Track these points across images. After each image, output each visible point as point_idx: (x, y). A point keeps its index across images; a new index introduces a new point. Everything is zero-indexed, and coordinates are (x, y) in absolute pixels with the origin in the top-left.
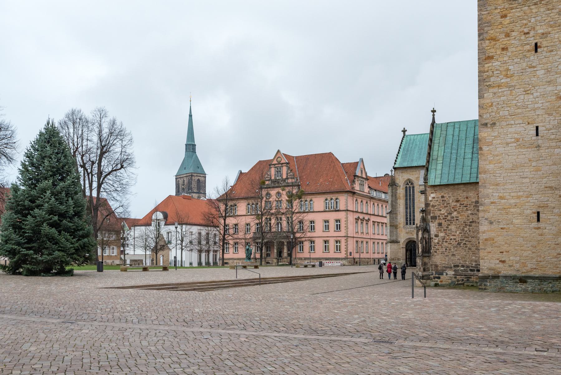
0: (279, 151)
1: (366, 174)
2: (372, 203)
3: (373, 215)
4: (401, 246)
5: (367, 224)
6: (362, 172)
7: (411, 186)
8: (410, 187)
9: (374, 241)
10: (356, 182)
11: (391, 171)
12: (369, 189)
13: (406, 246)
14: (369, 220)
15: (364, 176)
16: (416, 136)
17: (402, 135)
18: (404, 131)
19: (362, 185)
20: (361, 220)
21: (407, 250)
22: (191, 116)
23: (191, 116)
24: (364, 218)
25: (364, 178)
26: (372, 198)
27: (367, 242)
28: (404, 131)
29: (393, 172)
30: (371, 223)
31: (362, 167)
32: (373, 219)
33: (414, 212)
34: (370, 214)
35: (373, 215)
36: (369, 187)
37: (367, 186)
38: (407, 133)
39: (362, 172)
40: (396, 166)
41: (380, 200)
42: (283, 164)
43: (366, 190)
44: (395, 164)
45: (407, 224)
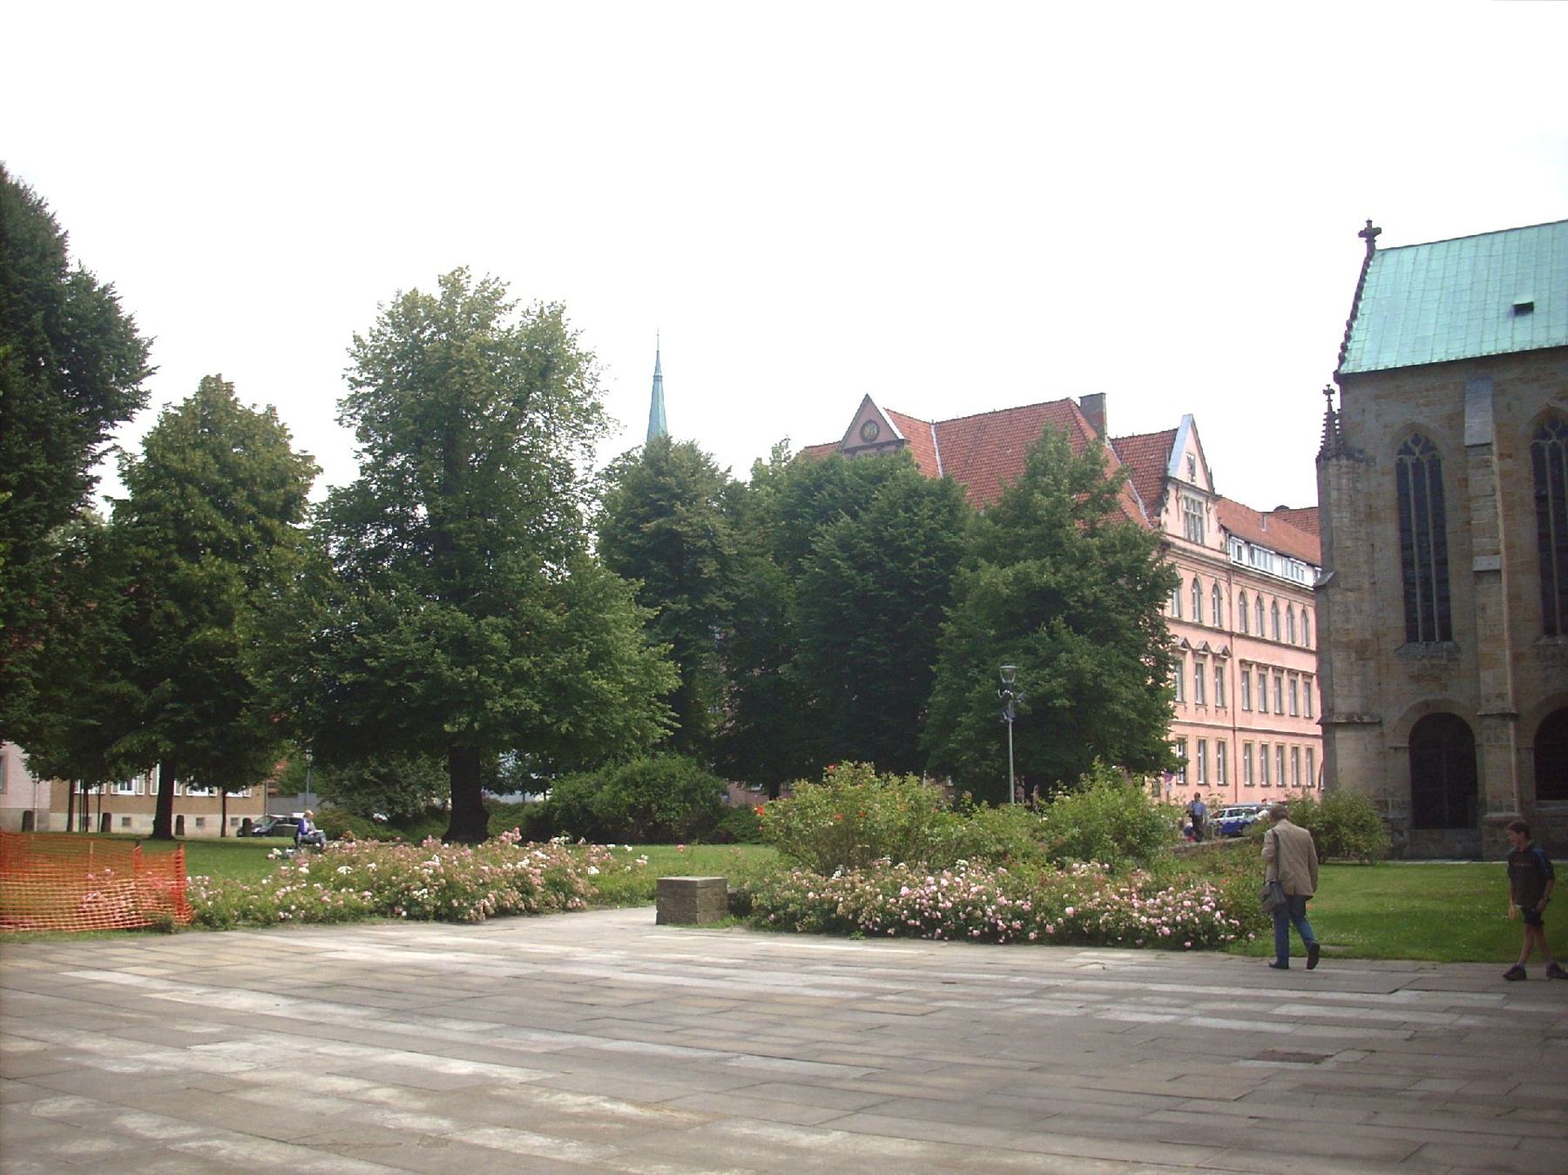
0: (867, 399)
1: (1209, 478)
2: (1236, 590)
3: (1240, 636)
4: (1391, 741)
5: (1219, 671)
6: (1192, 467)
7: (1425, 459)
8: (1417, 466)
9: (1248, 736)
10: (1171, 503)
11: (1329, 392)
12: (1221, 536)
13: (1412, 739)
14: (1222, 657)
15: (1201, 483)
16: (1424, 252)
17: (1364, 254)
18: (1370, 234)
19: (1193, 520)
20: (1195, 652)
21: (1416, 763)
22: (657, 378)
23: (657, 378)
24: (1206, 648)
25: (1199, 491)
26: (1234, 571)
27: (1221, 745)
28: (1370, 234)
29: (1336, 398)
30: (1232, 669)
31: (1194, 450)
32: (1242, 650)
33: (1443, 581)
34: (1231, 634)
35: (1240, 636)
36: (1223, 528)
37: (1214, 525)
38: (1381, 242)
39: (1192, 467)
40: (1345, 369)
41: (1266, 579)
42: (883, 445)
43: (1213, 537)
44: (1342, 359)
45: (1411, 635)
